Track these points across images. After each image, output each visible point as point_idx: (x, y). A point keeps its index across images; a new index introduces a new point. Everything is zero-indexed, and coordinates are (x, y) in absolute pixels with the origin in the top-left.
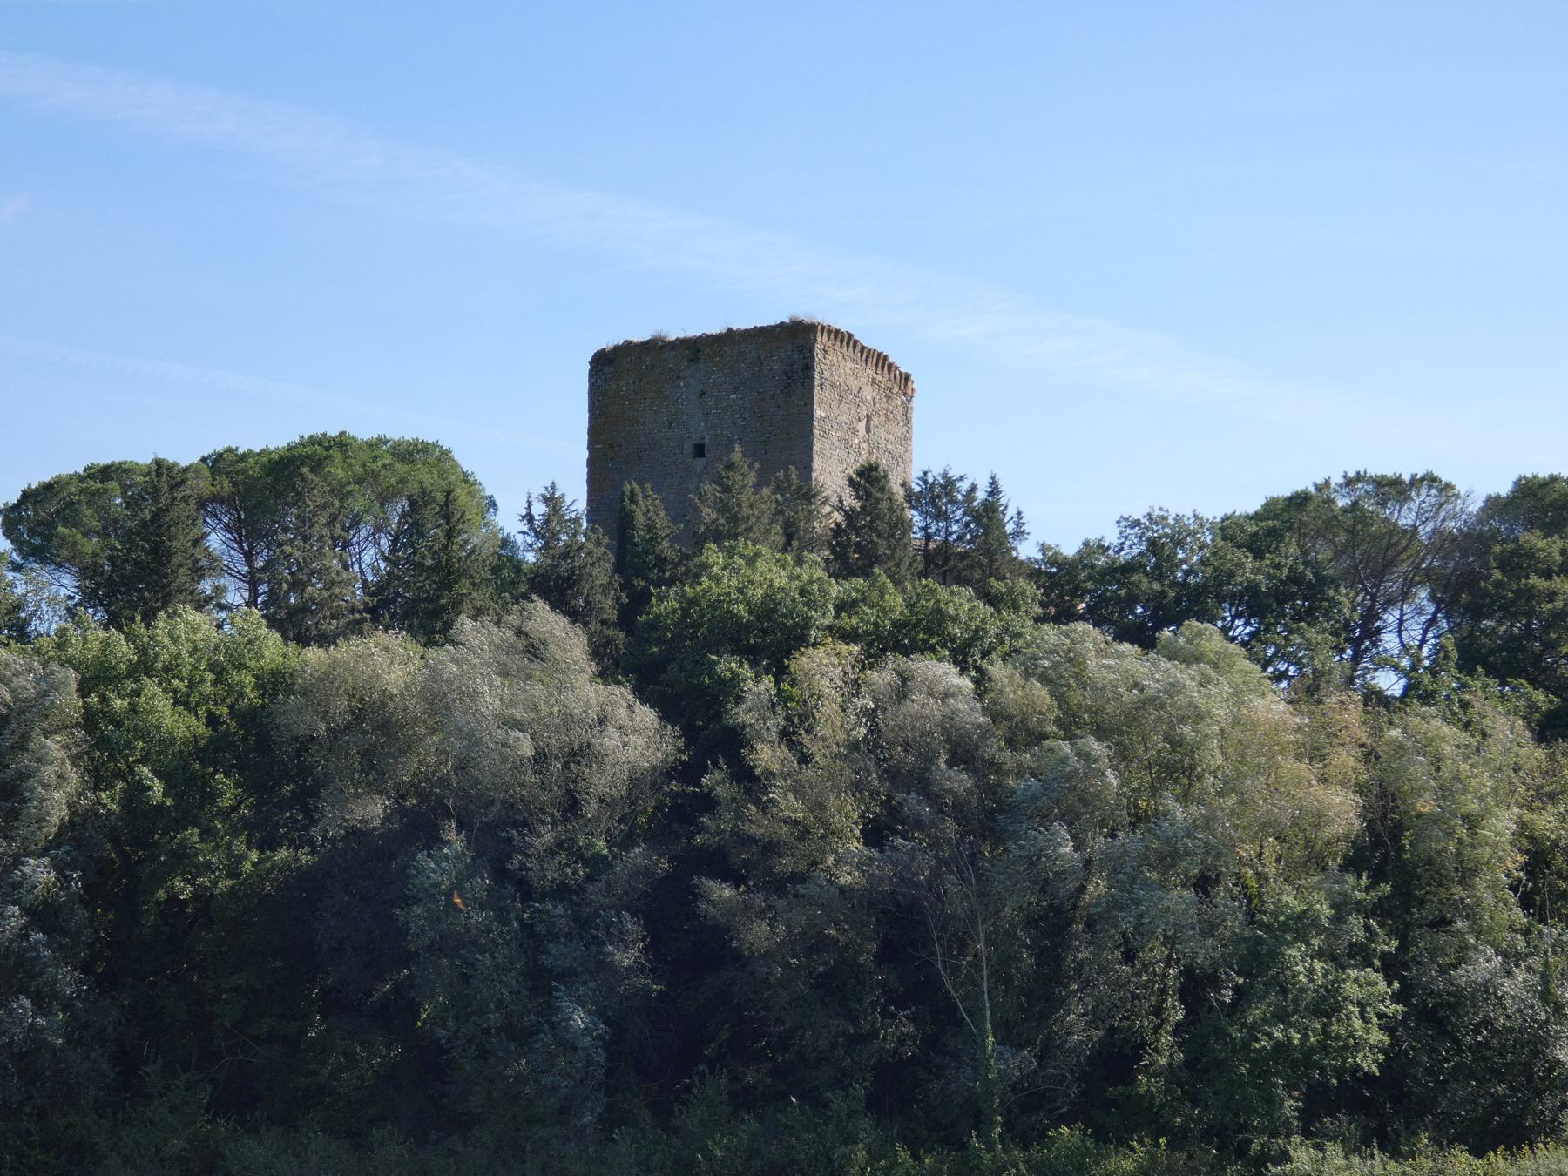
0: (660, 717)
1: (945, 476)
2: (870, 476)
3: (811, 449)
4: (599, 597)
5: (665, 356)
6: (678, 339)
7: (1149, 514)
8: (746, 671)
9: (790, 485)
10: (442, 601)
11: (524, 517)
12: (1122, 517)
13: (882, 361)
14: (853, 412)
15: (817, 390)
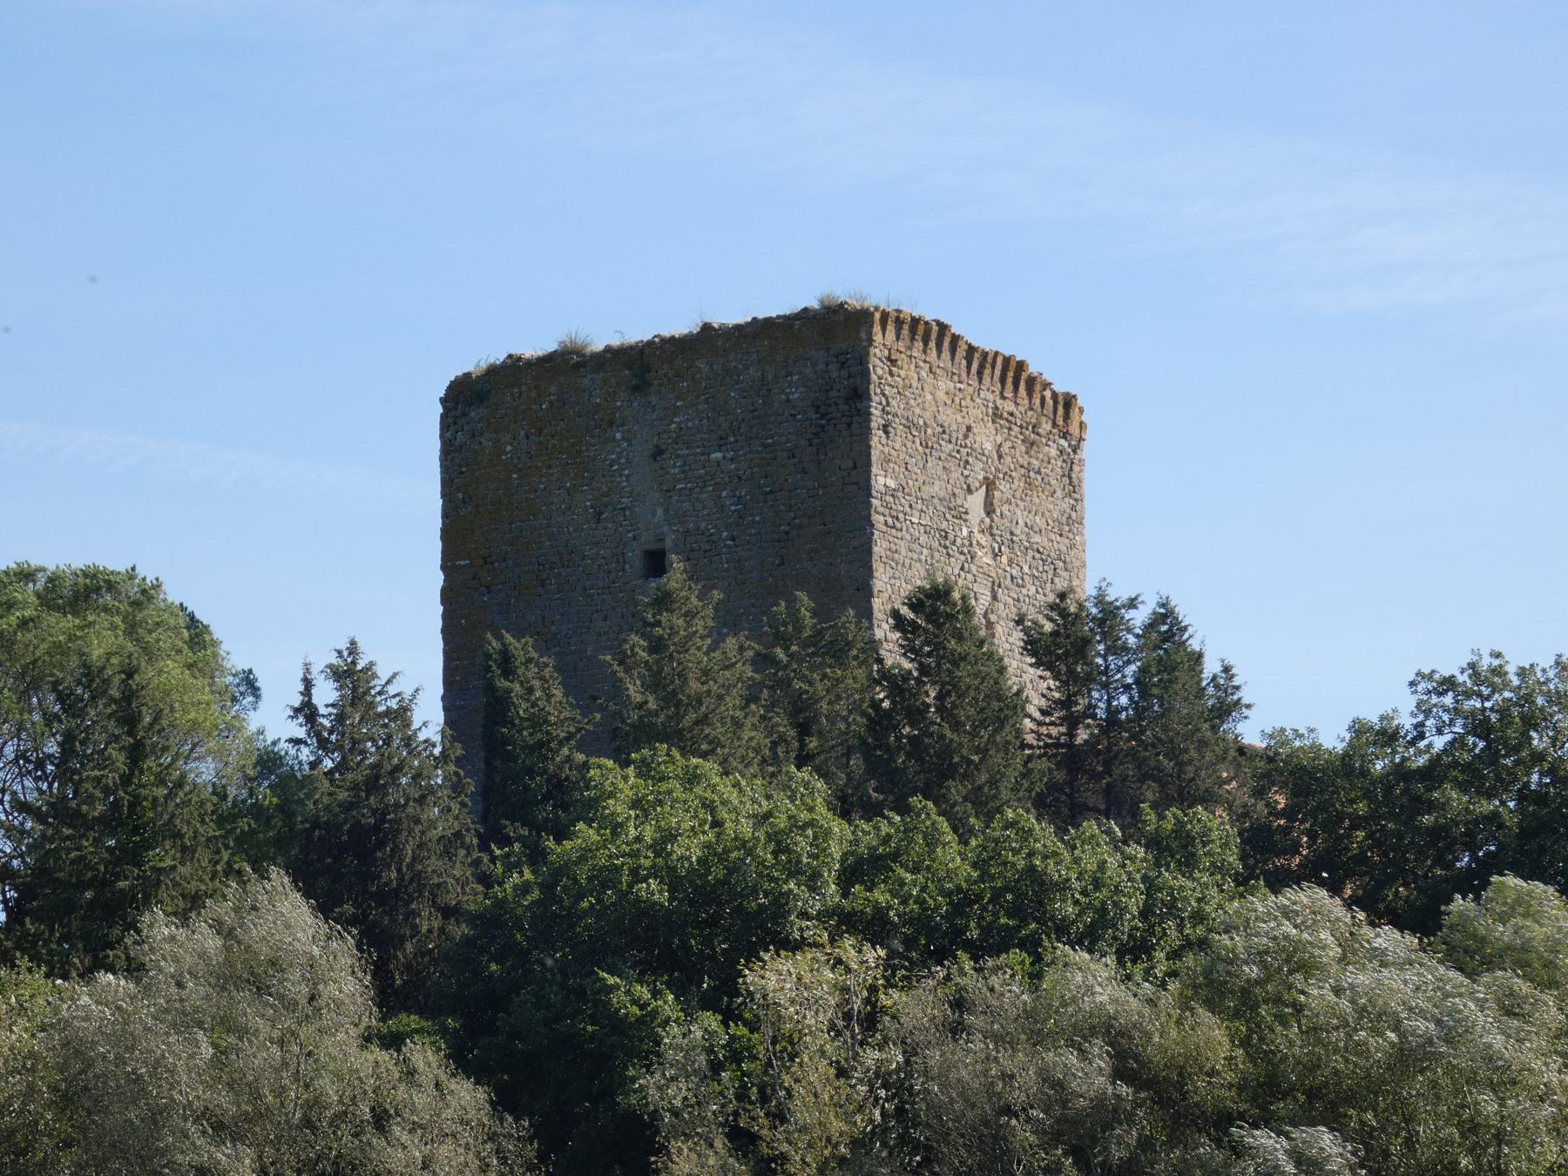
0: (492, 1103)
1: (1100, 600)
2: (935, 611)
3: (869, 552)
4: (434, 863)
5: (586, 382)
6: (608, 349)
7: (1472, 666)
8: (668, 1004)
9: (799, 629)
10: (122, 884)
11: (297, 711)
12: (1419, 674)
13: (1014, 373)
14: (955, 475)
15: (877, 438)
